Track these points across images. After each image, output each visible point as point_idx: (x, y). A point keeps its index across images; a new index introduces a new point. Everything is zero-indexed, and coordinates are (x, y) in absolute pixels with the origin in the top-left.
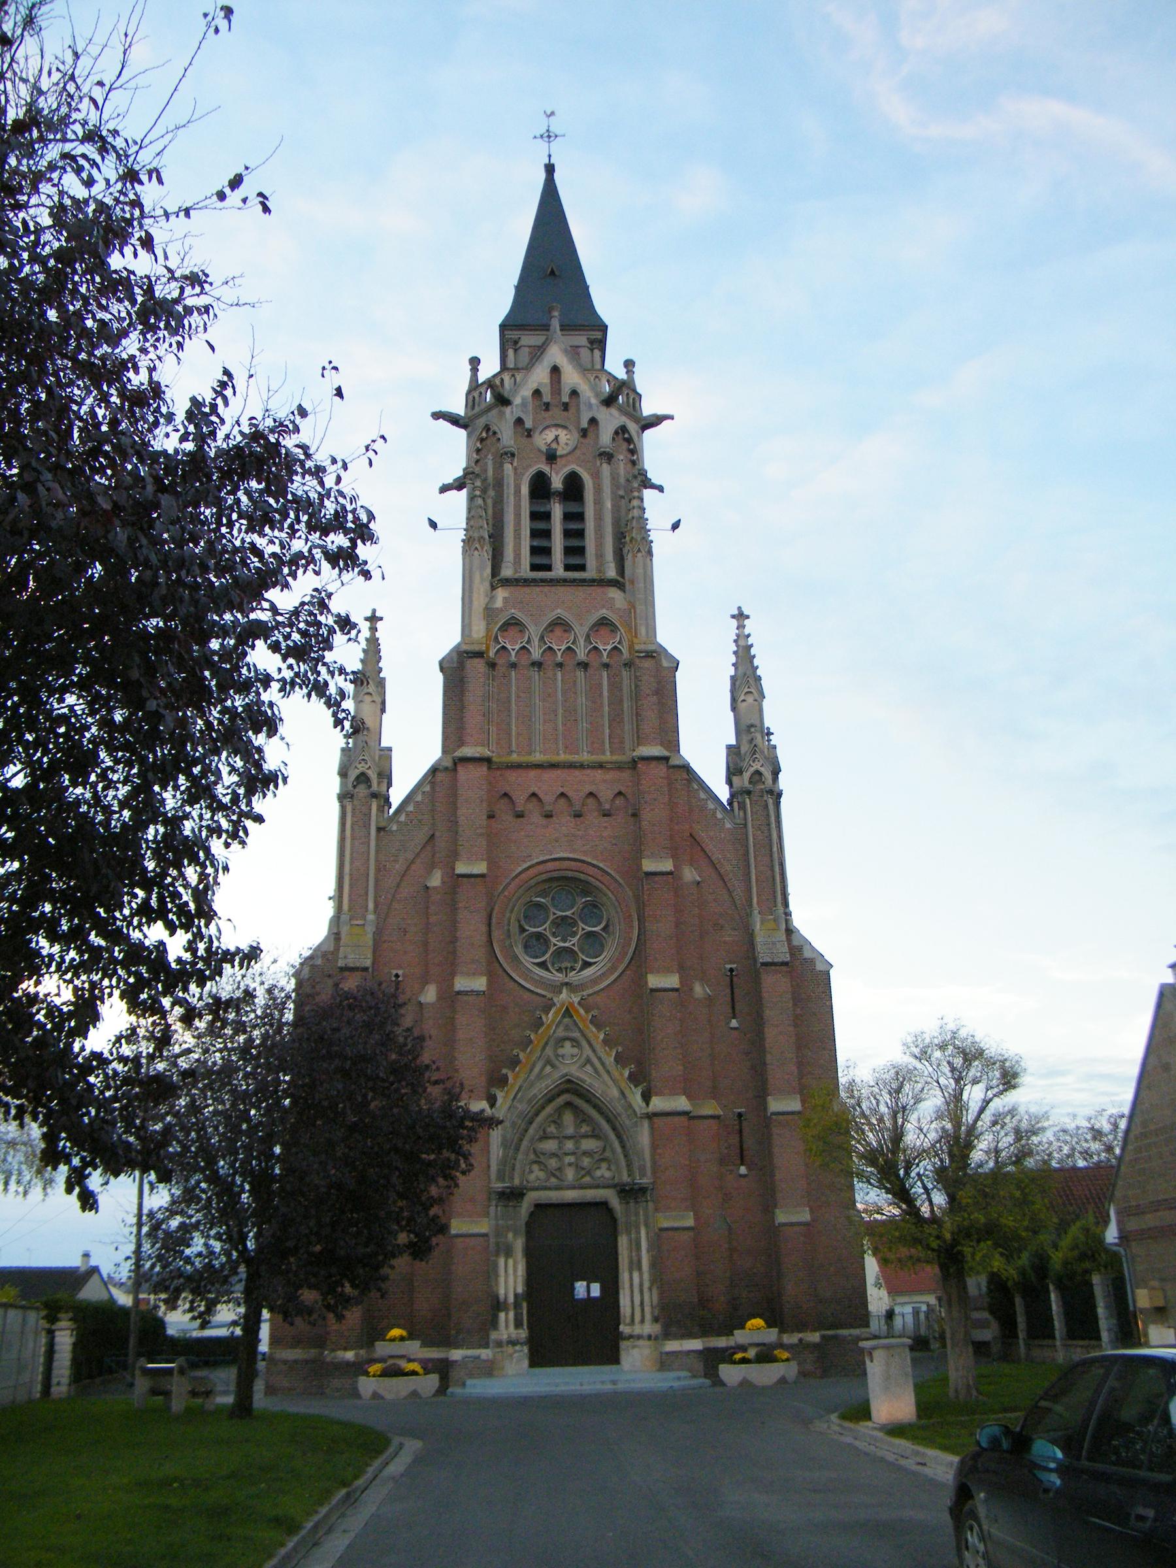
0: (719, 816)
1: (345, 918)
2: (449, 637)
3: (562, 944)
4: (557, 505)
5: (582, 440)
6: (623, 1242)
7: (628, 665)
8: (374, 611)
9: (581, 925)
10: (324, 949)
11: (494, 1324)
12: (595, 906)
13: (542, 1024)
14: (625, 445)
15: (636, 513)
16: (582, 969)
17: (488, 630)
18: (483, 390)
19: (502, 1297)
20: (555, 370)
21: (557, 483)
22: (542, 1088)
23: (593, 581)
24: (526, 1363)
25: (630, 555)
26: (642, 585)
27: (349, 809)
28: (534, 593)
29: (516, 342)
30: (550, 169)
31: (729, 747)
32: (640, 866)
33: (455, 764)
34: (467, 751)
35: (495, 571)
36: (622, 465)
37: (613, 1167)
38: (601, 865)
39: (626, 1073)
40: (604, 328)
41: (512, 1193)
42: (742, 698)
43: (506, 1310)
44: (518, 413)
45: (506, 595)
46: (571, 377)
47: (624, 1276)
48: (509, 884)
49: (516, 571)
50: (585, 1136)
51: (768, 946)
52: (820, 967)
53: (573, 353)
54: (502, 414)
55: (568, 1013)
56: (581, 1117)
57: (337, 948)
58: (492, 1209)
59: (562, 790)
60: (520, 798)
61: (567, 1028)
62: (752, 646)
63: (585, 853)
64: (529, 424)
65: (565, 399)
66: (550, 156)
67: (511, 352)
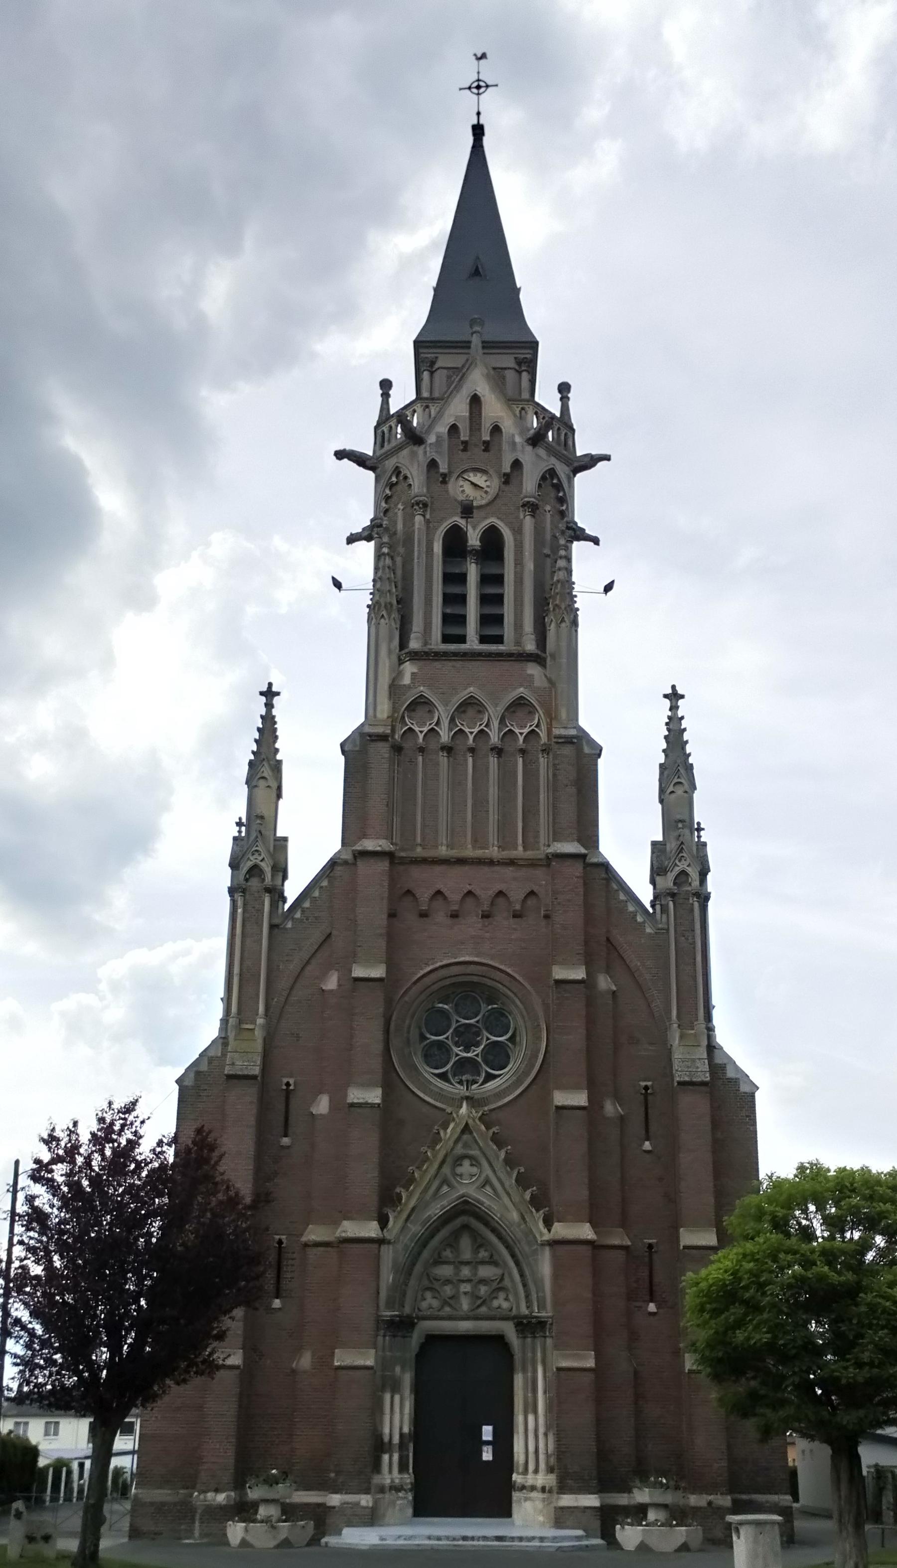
0: (639, 919)
1: (232, 1021)
2: (351, 716)
3: (465, 1055)
4: (473, 565)
5: (503, 486)
6: (519, 1380)
7: (546, 750)
8: (270, 685)
9: (486, 1034)
10: (212, 1053)
11: (377, 1467)
12: (503, 1015)
13: (440, 1140)
14: (553, 494)
15: (561, 575)
16: (485, 1081)
17: (394, 709)
18: (393, 423)
19: (386, 1439)
20: (475, 401)
21: (474, 539)
22: (436, 1210)
23: (510, 655)
24: (410, 1511)
25: (553, 625)
26: (564, 660)
27: (240, 903)
28: (446, 668)
29: (433, 363)
30: (478, 131)
31: (654, 844)
32: (550, 973)
33: (355, 857)
34: (370, 845)
35: (403, 645)
36: (548, 515)
37: (511, 1298)
38: (509, 970)
39: (527, 1195)
40: (534, 345)
41: (401, 1322)
42: (671, 789)
43: (390, 1452)
44: (432, 454)
45: (415, 670)
46: (494, 409)
47: (519, 1419)
48: (410, 988)
49: (426, 643)
50: (483, 1263)
51: (687, 1063)
52: (744, 1088)
53: (497, 377)
54: (414, 455)
55: (466, 1129)
56: (479, 1243)
57: (224, 1055)
58: (380, 1339)
59: (469, 888)
60: (424, 895)
61: (466, 1146)
62: (685, 730)
63: (492, 958)
64: (443, 468)
65: (486, 437)
66: (479, 114)
67: (426, 375)
